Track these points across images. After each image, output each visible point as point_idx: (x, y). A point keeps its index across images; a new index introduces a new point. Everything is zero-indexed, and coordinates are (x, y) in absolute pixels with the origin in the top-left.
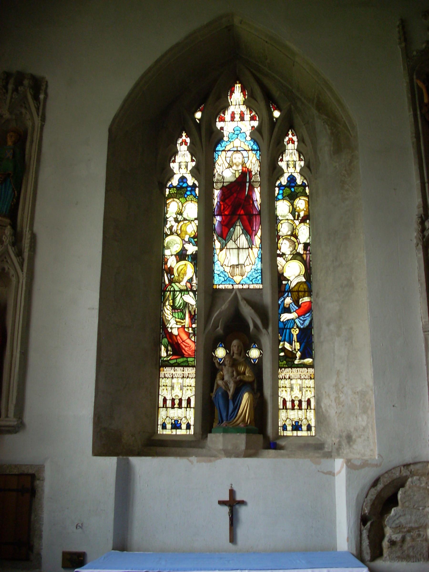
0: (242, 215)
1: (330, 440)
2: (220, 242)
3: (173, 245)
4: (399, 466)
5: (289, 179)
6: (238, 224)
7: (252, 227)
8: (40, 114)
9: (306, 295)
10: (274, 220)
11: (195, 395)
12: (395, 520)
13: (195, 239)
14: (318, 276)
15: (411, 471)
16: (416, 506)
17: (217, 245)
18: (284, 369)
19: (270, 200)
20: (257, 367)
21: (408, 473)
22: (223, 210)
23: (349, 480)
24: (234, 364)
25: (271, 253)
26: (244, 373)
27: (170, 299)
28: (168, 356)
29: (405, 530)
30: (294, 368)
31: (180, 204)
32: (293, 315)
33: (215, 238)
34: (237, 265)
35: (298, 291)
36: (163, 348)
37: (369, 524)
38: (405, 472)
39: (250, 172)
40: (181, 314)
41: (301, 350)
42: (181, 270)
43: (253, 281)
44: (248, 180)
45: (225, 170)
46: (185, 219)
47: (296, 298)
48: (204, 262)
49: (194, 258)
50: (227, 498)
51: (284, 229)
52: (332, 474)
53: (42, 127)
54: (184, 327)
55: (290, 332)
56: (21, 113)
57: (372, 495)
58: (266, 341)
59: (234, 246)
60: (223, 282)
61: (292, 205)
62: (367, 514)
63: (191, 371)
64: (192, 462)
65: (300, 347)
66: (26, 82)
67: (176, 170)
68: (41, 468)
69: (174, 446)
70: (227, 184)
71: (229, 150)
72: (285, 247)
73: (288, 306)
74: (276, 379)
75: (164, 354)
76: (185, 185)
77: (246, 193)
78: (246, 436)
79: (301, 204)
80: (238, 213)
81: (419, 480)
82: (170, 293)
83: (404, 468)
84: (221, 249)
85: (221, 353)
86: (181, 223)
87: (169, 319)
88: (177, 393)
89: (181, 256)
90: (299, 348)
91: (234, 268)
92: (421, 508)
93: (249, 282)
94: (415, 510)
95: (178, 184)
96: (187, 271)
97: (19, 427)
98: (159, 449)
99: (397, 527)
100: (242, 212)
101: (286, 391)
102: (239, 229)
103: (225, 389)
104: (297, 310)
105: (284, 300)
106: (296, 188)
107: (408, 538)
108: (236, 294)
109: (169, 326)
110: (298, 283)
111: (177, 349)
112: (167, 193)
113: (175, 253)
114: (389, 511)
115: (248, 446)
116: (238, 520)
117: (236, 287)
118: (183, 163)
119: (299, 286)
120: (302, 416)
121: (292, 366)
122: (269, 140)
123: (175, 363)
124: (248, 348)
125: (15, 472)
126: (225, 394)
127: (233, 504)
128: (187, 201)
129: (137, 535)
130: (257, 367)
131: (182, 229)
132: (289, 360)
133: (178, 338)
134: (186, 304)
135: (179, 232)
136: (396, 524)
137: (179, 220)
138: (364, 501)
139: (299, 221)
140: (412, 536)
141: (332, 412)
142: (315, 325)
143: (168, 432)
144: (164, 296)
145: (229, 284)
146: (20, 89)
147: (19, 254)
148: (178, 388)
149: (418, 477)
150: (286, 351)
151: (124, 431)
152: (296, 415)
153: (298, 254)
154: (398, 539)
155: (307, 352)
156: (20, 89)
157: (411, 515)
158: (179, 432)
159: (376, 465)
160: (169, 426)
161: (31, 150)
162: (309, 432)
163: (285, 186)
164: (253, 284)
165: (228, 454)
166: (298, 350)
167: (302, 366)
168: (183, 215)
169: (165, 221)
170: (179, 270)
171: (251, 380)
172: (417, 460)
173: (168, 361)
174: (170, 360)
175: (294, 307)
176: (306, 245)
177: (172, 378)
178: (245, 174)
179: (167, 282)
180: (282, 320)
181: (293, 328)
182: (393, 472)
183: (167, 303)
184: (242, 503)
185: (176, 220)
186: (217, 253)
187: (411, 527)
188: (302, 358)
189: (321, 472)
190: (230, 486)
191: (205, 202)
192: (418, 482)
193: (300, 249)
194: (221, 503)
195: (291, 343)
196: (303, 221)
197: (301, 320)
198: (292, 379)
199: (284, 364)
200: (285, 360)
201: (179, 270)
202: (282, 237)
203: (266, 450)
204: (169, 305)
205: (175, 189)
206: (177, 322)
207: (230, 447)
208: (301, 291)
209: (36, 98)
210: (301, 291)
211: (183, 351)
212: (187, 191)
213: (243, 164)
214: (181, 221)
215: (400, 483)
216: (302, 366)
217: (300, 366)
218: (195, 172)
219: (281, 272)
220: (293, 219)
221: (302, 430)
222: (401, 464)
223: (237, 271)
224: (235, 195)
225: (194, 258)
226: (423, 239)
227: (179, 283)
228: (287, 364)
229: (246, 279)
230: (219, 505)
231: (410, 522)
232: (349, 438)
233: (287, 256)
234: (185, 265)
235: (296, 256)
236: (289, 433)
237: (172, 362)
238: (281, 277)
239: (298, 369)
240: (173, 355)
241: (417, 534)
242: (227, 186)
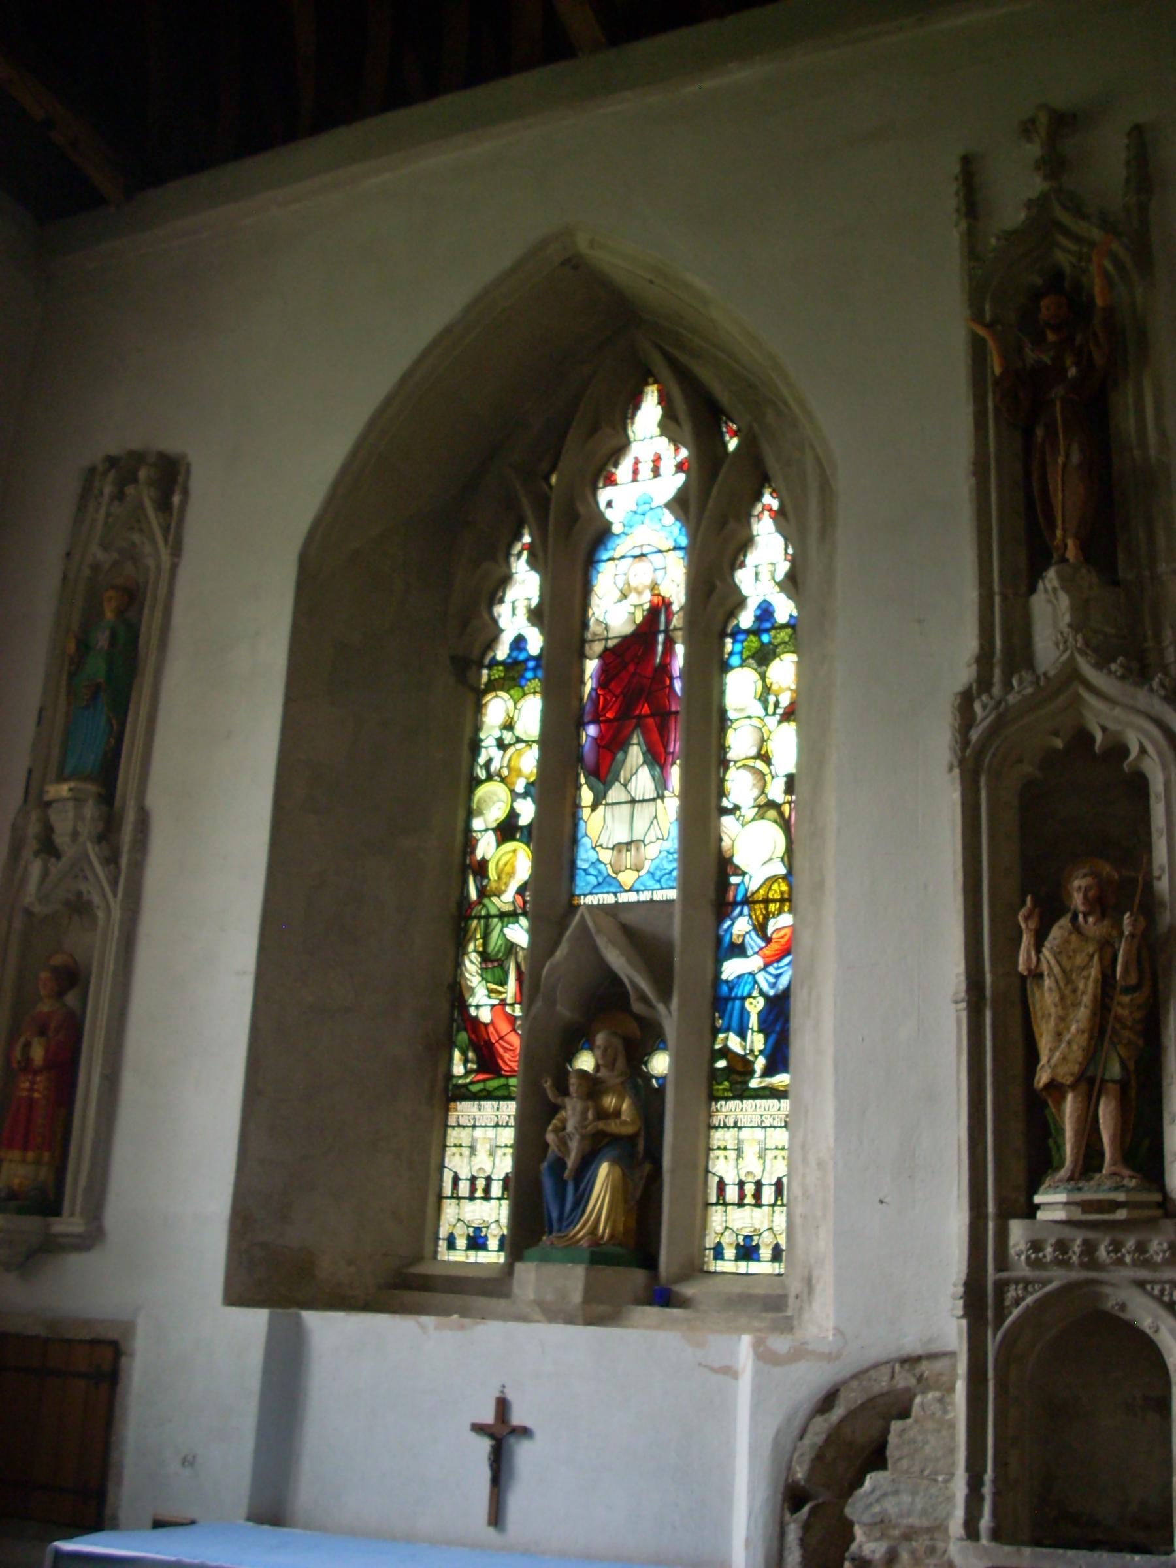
0: (647, 716)
2: (591, 788)
3: (493, 803)
4: (887, 1362)
5: (758, 612)
6: (635, 741)
7: (666, 746)
8: (171, 538)
9: (786, 909)
12: (871, 1504)
13: (541, 789)
15: (921, 1375)
16: (926, 1473)
18: (723, 1102)
19: (710, 669)
21: (913, 1381)
22: (604, 708)
23: (758, 1389)
25: (703, 810)
26: (617, 1113)
27: (478, 936)
28: (468, 1072)
29: (897, 1533)
30: (748, 1098)
31: (511, 703)
32: (752, 963)
33: (583, 780)
34: (628, 844)
35: (767, 901)
36: (457, 1054)
37: (806, 1509)
38: (904, 1380)
39: (668, 604)
40: (498, 972)
41: (767, 1052)
42: (506, 865)
43: (663, 881)
44: (662, 627)
45: (613, 610)
46: (519, 740)
47: (761, 918)
48: (554, 838)
49: (528, 835)
50: (488, 1416)
52: (730, 1372)
53: (174, 568)
54: (503, 1003)
55: (743, 1008)
56: (133, 545)
57: (817, 1434)
59: (624, 797)
60: (594, 887)
61: (763, 677)
62: (802, 1483)
63: (509, 1108)
64: (423, 1327)
65: (766, 1043)
66: (143, 474)
67: (745, 589)
68: (129, 1328)
69: (462, 1291)
70: (615, 641)
71: (623, 557)
72: (739, 787)
73: (740, 940)
75: (458, 1069)
76: (522, 656)
77: (658, 660)
78: (587, 1269)
79: (784, 671)
80: (637, 712)
81: (941, 1400)
82: (479, 923)
83: (902, 1367)
84: (594, 807)
86: (511, 750)
87: (473, 985)
88: (751, 1166)
89: (507, 830)
90: (762, 1047)
91: (620, 851)
92: (940, 1478)
93: (651, 883)
94: (925, 1482)
95: (509, 656)
97: (92, 1238)
98: (408, 1296)
99: (876, 1524)
100: (646, 710)
101: (726, 1157)
102: (635, 754)
103: (560, 1155)
104: (761, 949)
105: (733, 924)
106: (773, 633)
107: (905, 1556)
108: (582, 916)
109: (473, 1001)
110: (767, 880)
111: (487, 1059)
112: (484, 679)
113: (494, 825)
114: (860, 1482)
115: (589, 1296)
116: (511, 1474)
117: (624, 898)
119: (770, 889)
120: (762, 1223)
121: (743, 1093)
122: (713, 524)
123: (481, 1091)
125: (85, 1335)
126: (560, 1164)
127: (502, 1434)
128: (525, 694)
129: (308, 1490)
130: (650, 1098)
131: (512, 764)
132: (735, 1080)
133: (491, 1029)
134: (511, 948)
135: (505, 772)
136: (873, 1516)
137: (506, 742)
138: (795, 1449)
139: (778, 717)
140: (913, 1552)
143: (457, 1256)
144: (466, 930)
145: (608, 893)
146: (130, 490)
147: (112, 860)
149: (938, 1394)
150: (730, 1056)
152: (748, 1220)
153: (772, 805)
154: (877, 1556)
155: (778, 1060)
156: (130, 490)
157: (914, 1494)
158: (482, 1257)
159: (829, 1357)
160: (461, 1243)
162: (776, 1265)
163: (748, 632)
164: (662, 888)
165: (555, 1313)
166: (761, 1052)
167: (768, 1093)
169: (475, 746)
170: (501, 864)
171: (629, 1130)
172: (935, 1348)
173: (465, 1086)
174: (472, 1083)
177: (474, 1127)
178: (658, 609)
179: (473, 895)
180: (724, 977)
181: (749, 996)
182: (874, 1377)
183: (471, 947)
184: (525, 1432)
185: (501, 745)
186: (585, 817)
187: (911, 1527)
188: (769, 1072)
189: (705, 1366)
190: (499, 1388)
192: (938, 1406)
193: (776, 791)
194: (478, 1428)
195: (742, 1035)
197: (770, 974)
198: (740, 1128)
199: (725, 1090)
200: (727, 1080)
201: (501, 864)
202: (735, 762)
203: (639, 1308)
204: (475, 951)
205: (501, 668)
206: (490, 991)
207: (549, 1297)
208: (774, 901)
209: (164, 506)
210: (774, 901)
211: (500, 1062)
212: (526, 669)
213: (654, 587)
214: (510, 745)
216: (768, 1093)
217: (761, 1093)
218: (792, 583)
219: (727, 855)
220: (762, 713)
221: (758, 1260)
222: (894, 1355)
223: (628, 858)
224: (631, 668)
226: (963, 750)
227: (499, 897)
228: (730, 1090)
229: (647, 877)
230: (473, 1434)
231: (909, 1513)
233: (743, 811)
234: (514, 851)
236: (727, 1265)
237: (475, 1088)
238: (725, 866)
239: (758, 1102)
240: (477, 1071)
241: (927, 1547)
242: (615, 647)
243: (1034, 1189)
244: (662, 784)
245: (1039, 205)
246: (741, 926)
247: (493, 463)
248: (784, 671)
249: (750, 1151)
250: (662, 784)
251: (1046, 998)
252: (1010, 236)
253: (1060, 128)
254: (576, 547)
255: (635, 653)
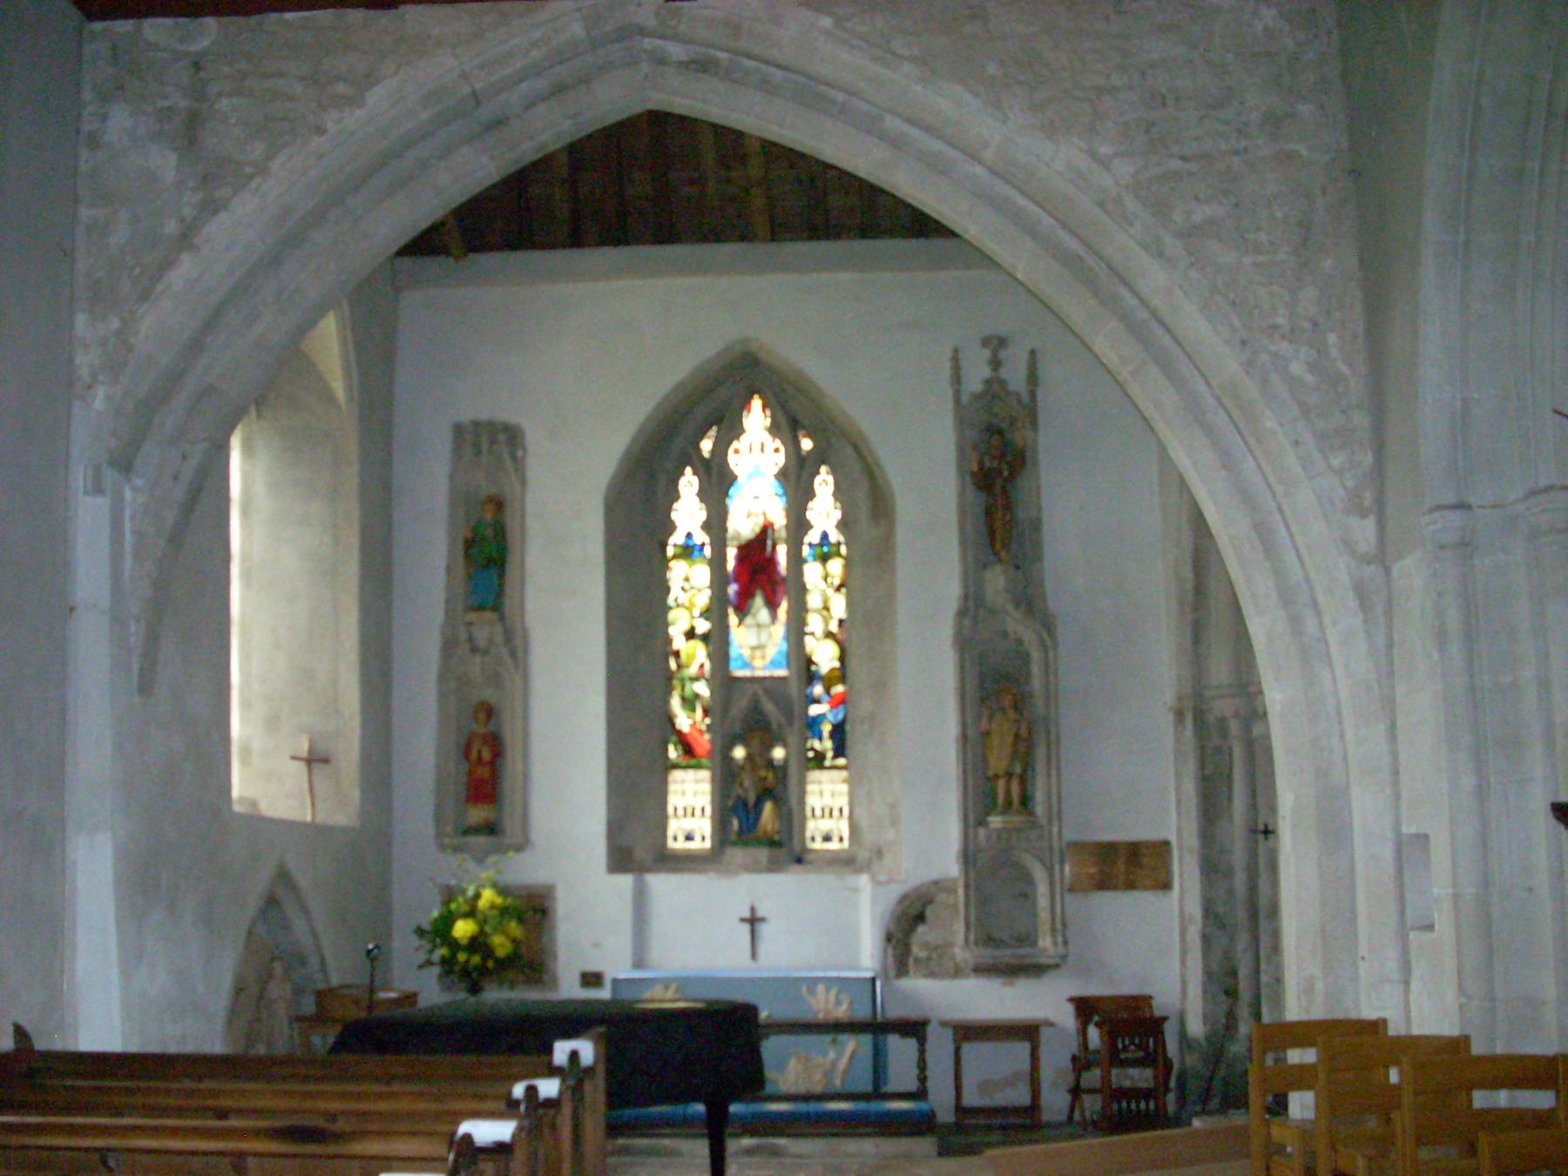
1: (863, 855)
10: (802, 590)
11: (713, 802)
13: (706, 614)
14: (853, 662)
17: (733, 619)
19: (797, 561)
20: (781, 771)
23: (874, 896)
24: (754, 767)
45: (742, 524)
48: (717, 641)
49: (705, 638)
51: (813, 601)
52: (856, 890)
58: (792, 739)
72: (814, 623)
74: (802, 783)
79: (836, 566)
85: (739, 753)
88: (828, 801)
89: (690, 634)
96: (696, 656)
102: (759, 601)
111: (688, 749)
118: (688, 513)
121: (821, 767)
122: (797, 483)
124: (770, 747)
127: (753, 921)
134: (697, 696)
141: (864, 822)
142: (849, 720)
146: (495, 447)
148: (690, 800)
151: (636, 845)
155: (839, 751)
161: (512, 523)
168: (689, 587)
169: (668, 590)
175: (826, 698)
176: (841, 622)
178: (766, 529)
184: (763, 920)
188: (836, 756)
191: (717, 563)
194: (743, 920)
196: (838, 589)
215: (930, 901)
223: (758, 653)
225: (705, 638)
232: (879, 853)
235: (829, 635)
243: (988, 814)
244: (774, 617)
245: (989, 382)
246: (818, 690)
247: (678, 440)
248: (836, 566)
249: (827, 795)
250: (774, 617)
251: (995, 741)
252: (977, 397)
253: (996, 344)
254: (717, 483)
255: (756, 554)
